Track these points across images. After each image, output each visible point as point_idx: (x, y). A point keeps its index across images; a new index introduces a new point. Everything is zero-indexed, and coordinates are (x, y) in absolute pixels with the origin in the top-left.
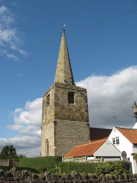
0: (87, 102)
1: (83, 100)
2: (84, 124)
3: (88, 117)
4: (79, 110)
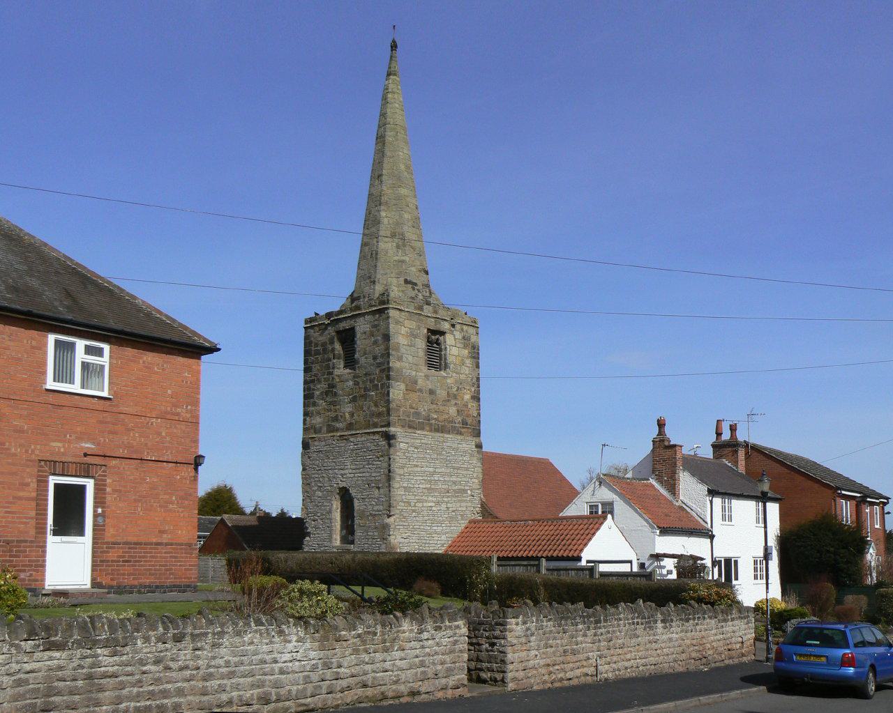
0: (478, 366)
1: (468, 362)
2: (468, 445)
3: (479, 421)
4: (455, 397)
